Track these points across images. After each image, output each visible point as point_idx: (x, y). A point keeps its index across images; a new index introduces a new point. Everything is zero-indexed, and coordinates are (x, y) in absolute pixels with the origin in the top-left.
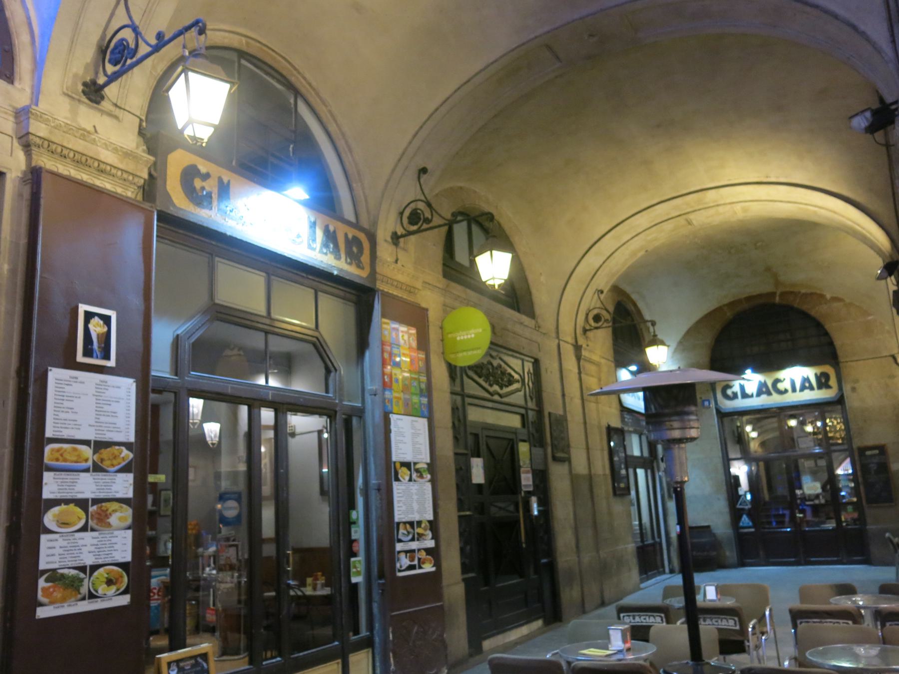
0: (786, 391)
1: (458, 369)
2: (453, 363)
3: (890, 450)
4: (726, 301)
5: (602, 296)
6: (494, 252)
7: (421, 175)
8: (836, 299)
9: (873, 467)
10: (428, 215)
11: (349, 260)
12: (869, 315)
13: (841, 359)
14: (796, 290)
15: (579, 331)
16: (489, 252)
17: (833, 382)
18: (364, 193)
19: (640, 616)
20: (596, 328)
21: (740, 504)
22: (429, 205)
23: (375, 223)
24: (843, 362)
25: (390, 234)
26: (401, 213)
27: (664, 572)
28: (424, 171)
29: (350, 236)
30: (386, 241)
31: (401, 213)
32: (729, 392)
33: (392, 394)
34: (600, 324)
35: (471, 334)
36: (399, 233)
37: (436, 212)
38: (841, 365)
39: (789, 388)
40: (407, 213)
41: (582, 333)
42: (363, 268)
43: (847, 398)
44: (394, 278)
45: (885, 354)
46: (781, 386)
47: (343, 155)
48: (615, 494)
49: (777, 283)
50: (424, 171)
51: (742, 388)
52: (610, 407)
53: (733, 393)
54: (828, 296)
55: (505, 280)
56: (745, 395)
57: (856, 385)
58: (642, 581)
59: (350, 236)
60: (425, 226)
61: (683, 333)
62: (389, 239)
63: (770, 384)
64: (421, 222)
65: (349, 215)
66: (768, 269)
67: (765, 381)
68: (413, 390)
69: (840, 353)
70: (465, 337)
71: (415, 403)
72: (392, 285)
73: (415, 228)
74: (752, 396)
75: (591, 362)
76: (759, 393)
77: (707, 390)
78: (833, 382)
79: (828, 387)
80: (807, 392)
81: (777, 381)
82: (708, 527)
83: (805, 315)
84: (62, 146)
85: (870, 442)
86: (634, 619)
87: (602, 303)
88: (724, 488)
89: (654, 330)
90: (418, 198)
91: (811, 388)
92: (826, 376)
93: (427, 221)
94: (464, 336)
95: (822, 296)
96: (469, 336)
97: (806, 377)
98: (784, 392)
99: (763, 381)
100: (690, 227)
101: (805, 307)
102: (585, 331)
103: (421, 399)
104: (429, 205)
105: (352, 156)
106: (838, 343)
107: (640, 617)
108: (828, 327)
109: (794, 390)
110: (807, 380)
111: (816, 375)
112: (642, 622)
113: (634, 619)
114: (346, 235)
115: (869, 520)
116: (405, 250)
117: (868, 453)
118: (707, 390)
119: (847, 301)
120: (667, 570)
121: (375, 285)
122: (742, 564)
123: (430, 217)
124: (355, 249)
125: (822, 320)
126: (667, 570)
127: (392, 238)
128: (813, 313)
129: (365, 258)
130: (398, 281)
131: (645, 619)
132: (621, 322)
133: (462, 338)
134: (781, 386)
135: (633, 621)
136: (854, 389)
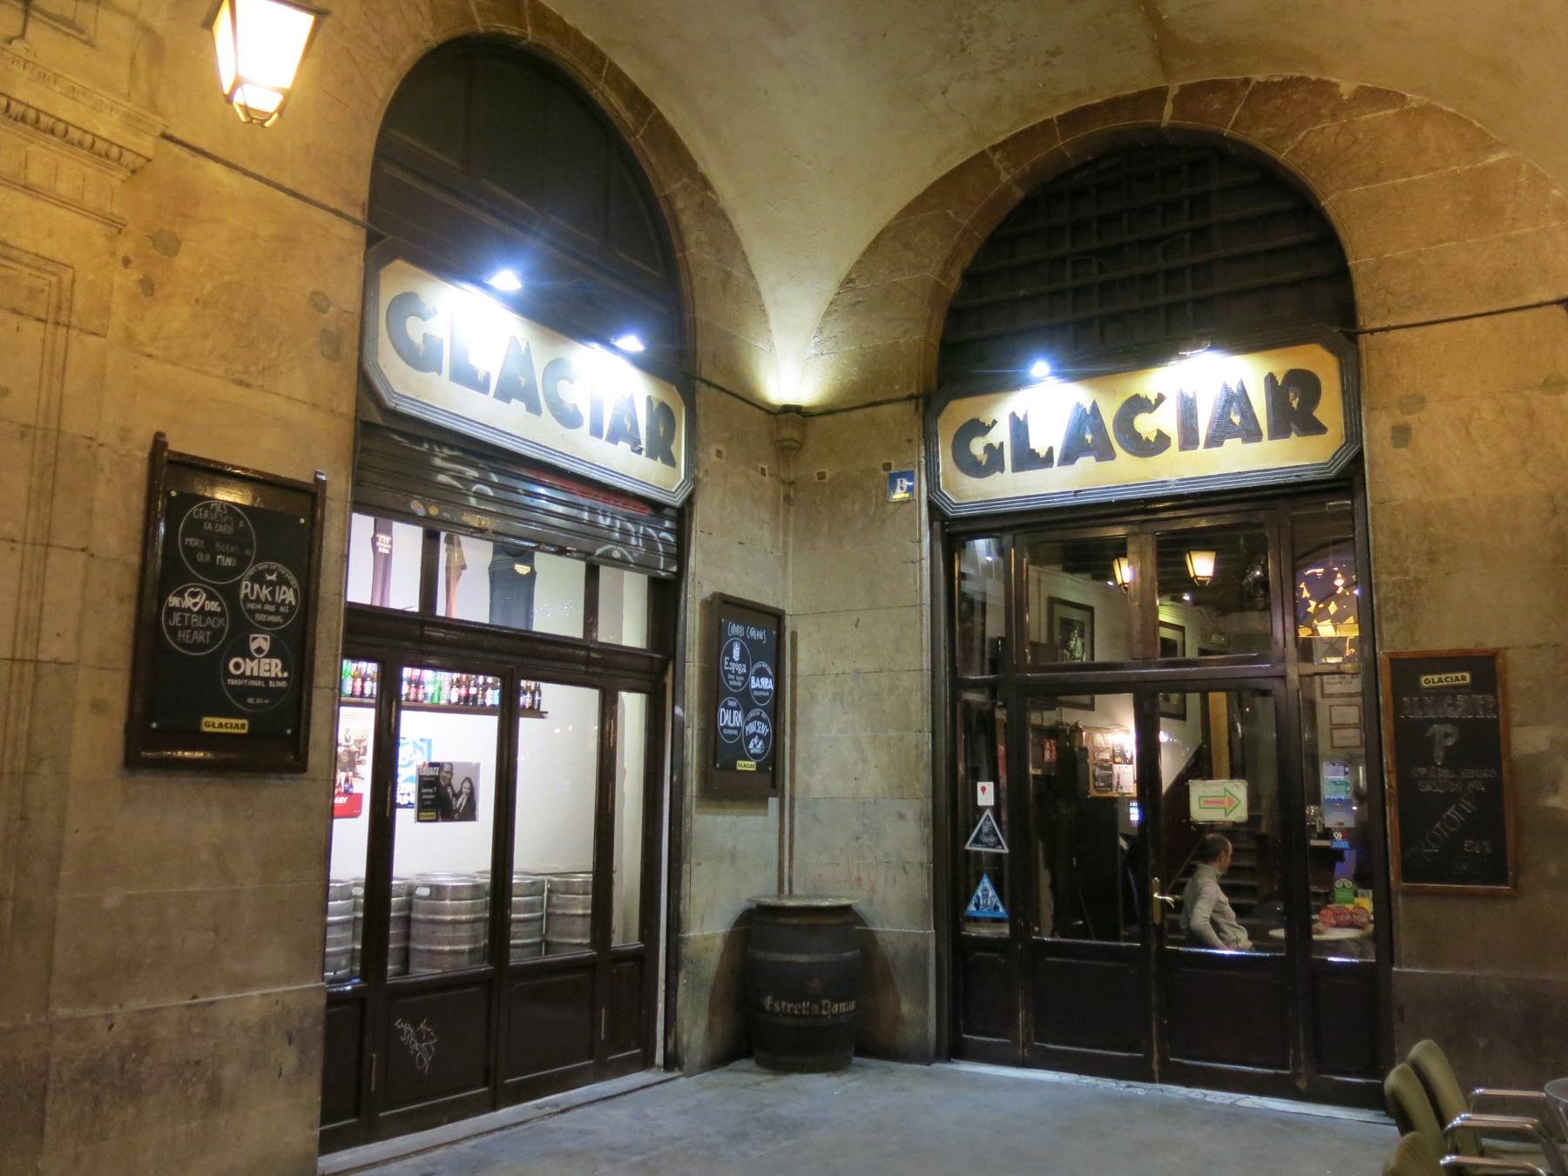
0: (1162, 441)
1: (1252, 814)
3: (1519, 675)
4: (1001, 131)
8: (1375, 96)
9: (1444, 736)
12: (1492, 147)
13: (1365, 321)
17: (1329, 409)
21: (977, 841)
24: (1372, 332)
27: (646, 1062)
32: (977, 447)
38: (1365, 341)
39: (1172, 431)
43: (1372, 465)
45: (1534, 298)
46: (1146, 425)
48: (429, 742)
49: (1166, 43)
51: (1019, 428)
53: (989, 448)
54: (1346, 88)
56: (1027, 459)
57: (1412, 419)
58: (330, 1143)
61: (856, 256)
63: (1108, 417)
67: (1095, 408)
74: (1047, 461)
77: (909, 441)
78: (1329, 409)
79: (1313, 427)
80: (1233, 444)
81: (1138, 405)
82: (845, 910)
84: (94, 135)
85: (1445, 642)
88: (926, 777)
91: (1250, 433)
92: (1304, 384)
95: (1323, 88)
101: (1256, 137)
106: (1360, 261)
108: (1331, 202)
109: (1189, 439)
110: (1239, 399)
111: (1271, 378)
115: (1405, 942)
117: (1429, 681)
119: (1415, 99)
120: (659, 1058)
122: (954, 1049)
125: (1311, 178)
126: (659, 1058)
128: (1283, 155)
134: (1146, 425)
136: (1402, 435)
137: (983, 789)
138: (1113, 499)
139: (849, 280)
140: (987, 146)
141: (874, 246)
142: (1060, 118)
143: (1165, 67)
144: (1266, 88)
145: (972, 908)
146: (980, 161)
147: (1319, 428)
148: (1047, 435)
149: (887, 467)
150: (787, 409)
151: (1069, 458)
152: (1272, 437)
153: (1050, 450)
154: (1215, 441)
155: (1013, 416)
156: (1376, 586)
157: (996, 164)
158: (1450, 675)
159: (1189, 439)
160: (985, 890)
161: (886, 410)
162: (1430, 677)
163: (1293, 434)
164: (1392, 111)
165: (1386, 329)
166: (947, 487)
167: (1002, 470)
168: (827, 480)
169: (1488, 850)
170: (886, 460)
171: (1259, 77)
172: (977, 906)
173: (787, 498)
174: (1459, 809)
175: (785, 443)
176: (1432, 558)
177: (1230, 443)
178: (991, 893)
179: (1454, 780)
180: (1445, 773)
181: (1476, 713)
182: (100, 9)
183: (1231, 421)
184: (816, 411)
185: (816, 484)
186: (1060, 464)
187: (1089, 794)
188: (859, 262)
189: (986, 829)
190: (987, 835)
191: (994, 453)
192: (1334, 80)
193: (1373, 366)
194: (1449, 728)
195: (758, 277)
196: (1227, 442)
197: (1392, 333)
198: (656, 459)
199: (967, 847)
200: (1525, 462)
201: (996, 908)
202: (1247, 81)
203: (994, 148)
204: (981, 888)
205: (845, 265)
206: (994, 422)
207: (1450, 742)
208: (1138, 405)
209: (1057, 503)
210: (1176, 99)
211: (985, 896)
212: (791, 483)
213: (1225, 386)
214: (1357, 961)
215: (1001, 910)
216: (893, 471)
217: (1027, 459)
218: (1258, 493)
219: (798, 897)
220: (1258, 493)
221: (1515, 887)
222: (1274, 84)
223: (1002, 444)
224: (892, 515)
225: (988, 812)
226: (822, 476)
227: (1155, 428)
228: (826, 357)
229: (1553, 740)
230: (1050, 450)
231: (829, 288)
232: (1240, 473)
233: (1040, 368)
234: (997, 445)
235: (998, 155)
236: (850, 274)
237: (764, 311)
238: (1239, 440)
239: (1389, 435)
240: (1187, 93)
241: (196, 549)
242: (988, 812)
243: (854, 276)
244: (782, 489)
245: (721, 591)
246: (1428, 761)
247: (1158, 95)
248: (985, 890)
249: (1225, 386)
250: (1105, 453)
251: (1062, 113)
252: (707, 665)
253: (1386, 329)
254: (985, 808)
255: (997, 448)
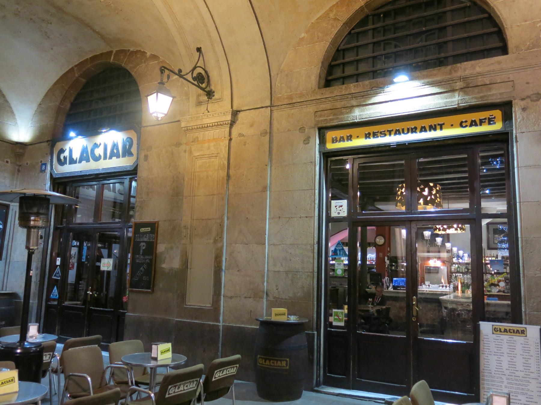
3: (161, 230)
6: (159, 94)
16: (156, 94)
21: (55, 276)
54: (148, 54)
55: (166, 115)
57: (149, 153)
77: (47, 154)
81: (96, 146)
86: (265, 362)
89: (504, 249)
95: (144, 53)
97: (116, 142)
98: (97, 159)
99: (85, 146)
107: (270, 361)
109: (105, 158)
112: (271, 365)
113: (265, 362)
117: (142, 230)
118: (47, 154)
131: (273, 363)
135: (264, 363)
137: (58, 260)
138: (88, 174)
139: (40, 104)
140: (74, 65)
141: (46, 95)
142: (90, 58)
144: (132, 52)
146: (72, 70)
148: (76, 155)
149: (41, 162)
150: (17, 143)
152: (122, 157)
155: (70, 147)
157: (75, 71)
161: (43, 144)
163: (127, 156)
164: (156, 62)
166: (55, 169)
167: (66, 164)
169: (148, 280)
171: (131, 49)
172: (53, 295)
173: (19, 171)
174: (143, 268)
175: (18, 153)
176: (148, 194)
177: (114, 158)
179: (143, 259)
180: (142, 257)
181: (150, 240)
183: (114, 152)
184: (28, 144)
186: (79, 163)
187: (384, 279)
188: (43, 99)
189: (57, 272)
190: (57, 274)
191: (65, 158)
192: (146, 51)
194: (144, 244)
195: (10, 102)
198: (125, 157)
199: (53, 277)
200: (169, 167)
202: (129, 50)
203: (76, 66)
205: (39, 99)
206: (66, 149)
207: (144, 248)
208: (96, 146)
209: (76, 174)
210: (115, 54)
211: (55, 292)
212: (20, 166)
213: (114, 142)
214: (465, 342)
216: (43, 163)
217: (72, 161)
218: (122, 173)
219: (7, 291)
220: (122, 173)
221: (153, 291)
222: (134, 51)
225: (58, 267)
227: (98, 153)
228: (32, 127)
229: (165, 248)
230: (77, 158)
231: (35, 106)
232: (115, 167)
233: (72, 134)
234: (66, 156)
236: (41, 102)
237: (13, 113)
238: (115, 157)
239: (143, 157)
241: (437, 190)
242: (58, 267)
243: (41, 103)
244: (17, 167)
246: (139, 254)
249: (114, 142)
250: (88, 161)
251: (90, 56)
254: (58, 265)
255: (98, 156)
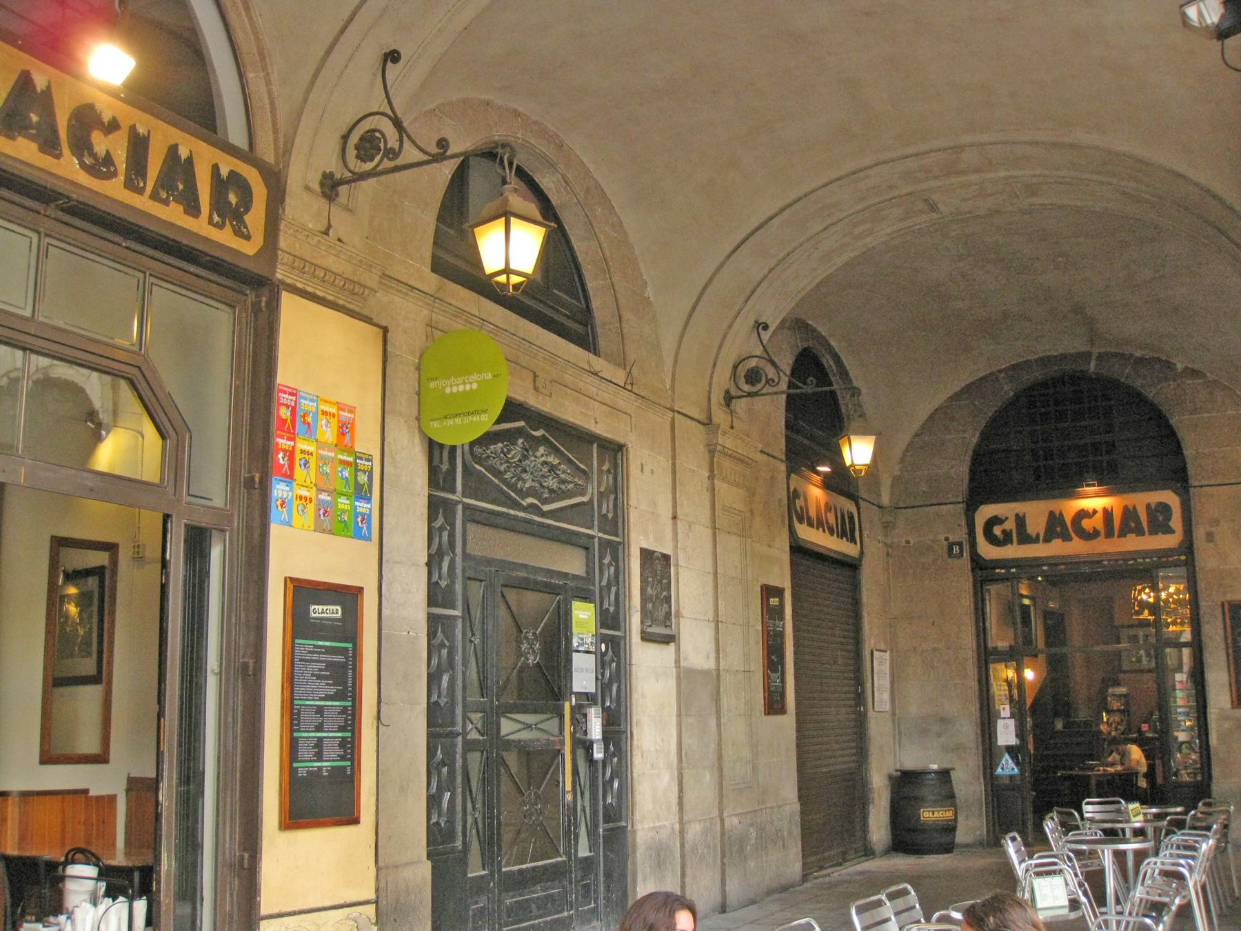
2: (438, 439)
5: (766, 336)
7: (389, 64)
8: (1194, 373)
10: (393, 142)
11: (216, 218)
13: (1192, 482)
14: (1127, 350)
15: (717, 397)
17: (1176, 522)
18: (270, 92)
19: (938, 811)
20: (750, 395)
22: (397, 123)
23: (285, 152)
24: (1195, 487)
25: (319, 177)
26: (345, 138)
28: (393, 56)
29: (224, 172)
30: (307, 188)
31: (345, 138)
32: (997, 531)
33: (291, 490)
34: (759, 386)
35: (471, 383)
36: (338, 176)
37: (409, 137)
38: (1192, 490)
39: (1100, 526)
40: (354, 139)
41: (723, 402)
42: (248, 238)
44: (319, 262)
46: (1087, 524)
47: (232, 16)
50: (393, 56)
52: (769, 546)
53: (1004, 532)
54: (1179, 367)
59: (224, 172)
60: (387, 164)
62: (316, 186)
64: (378, 158)
65: (237, 137)
66: (1078, 309)
68: (340, 486)
69: (1191, 470)
70: (461, 388)
71: (344, 511)
72: (313, 275)
73: (369, 166)
75: (735, 458)
76: (1049, 536)
78: (1176, 522)
83: (1137, 399)
86: (933, 814)
87: (765, 350)
90: (381, 110)
93: (392, 154)
94: (458, 385)
95: (1169, 365)
96: (468, 387)
100: (934, 216)
102: (729, 399)
103: (357, 503)
104: (397, 123)
105: (250, 19)
113: (933, 814)
114: (216, 168)
116: (347, 209)
121: (274, 272)
123: (396, 147)
124: (233, 198)
125: (1164, 408)
127: (322, 184)
129: (255, 218)
130: (326, 270)
132: (801, 388)
133: (455, 389)
136: (1210, 537)
137: (1004, 709)
143: (1092, 342)
145: (999, 770)
147: (1171, 531)
151: (1047, 540)
152: (1151, 533)
153: (1038, 535)
154: (1123, 534)
156: (758, 642)
158: (329, 607)
159: (1109, 533)
160: (1007, 760)
162: (316, 607)
164: (1200, 381)
165: (1201, 486)
168: (911, 545)
170: (946, 535)
172: (1003, 769)
178: (1010, 761)
182: (332, 204)
185: (905, 547)
193: (1196, 504)
196: (1128, 535)
197: (1204, 489)
201: (1013, 769)
204: (1004, 759)
211: (1007, 764)
215: (1016, 770)
223: (1011, 530)
224: (625, 917)
226: (908, 542)
230: (1038, 535)
235: (1002, 375)
239: (1204, 537)
240: (1100, 357)
245: (248, 179)
247: (1088, 355)
248: (1007, 760)
252: (61, 885)
253: (1201, 486)
